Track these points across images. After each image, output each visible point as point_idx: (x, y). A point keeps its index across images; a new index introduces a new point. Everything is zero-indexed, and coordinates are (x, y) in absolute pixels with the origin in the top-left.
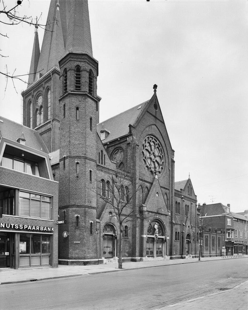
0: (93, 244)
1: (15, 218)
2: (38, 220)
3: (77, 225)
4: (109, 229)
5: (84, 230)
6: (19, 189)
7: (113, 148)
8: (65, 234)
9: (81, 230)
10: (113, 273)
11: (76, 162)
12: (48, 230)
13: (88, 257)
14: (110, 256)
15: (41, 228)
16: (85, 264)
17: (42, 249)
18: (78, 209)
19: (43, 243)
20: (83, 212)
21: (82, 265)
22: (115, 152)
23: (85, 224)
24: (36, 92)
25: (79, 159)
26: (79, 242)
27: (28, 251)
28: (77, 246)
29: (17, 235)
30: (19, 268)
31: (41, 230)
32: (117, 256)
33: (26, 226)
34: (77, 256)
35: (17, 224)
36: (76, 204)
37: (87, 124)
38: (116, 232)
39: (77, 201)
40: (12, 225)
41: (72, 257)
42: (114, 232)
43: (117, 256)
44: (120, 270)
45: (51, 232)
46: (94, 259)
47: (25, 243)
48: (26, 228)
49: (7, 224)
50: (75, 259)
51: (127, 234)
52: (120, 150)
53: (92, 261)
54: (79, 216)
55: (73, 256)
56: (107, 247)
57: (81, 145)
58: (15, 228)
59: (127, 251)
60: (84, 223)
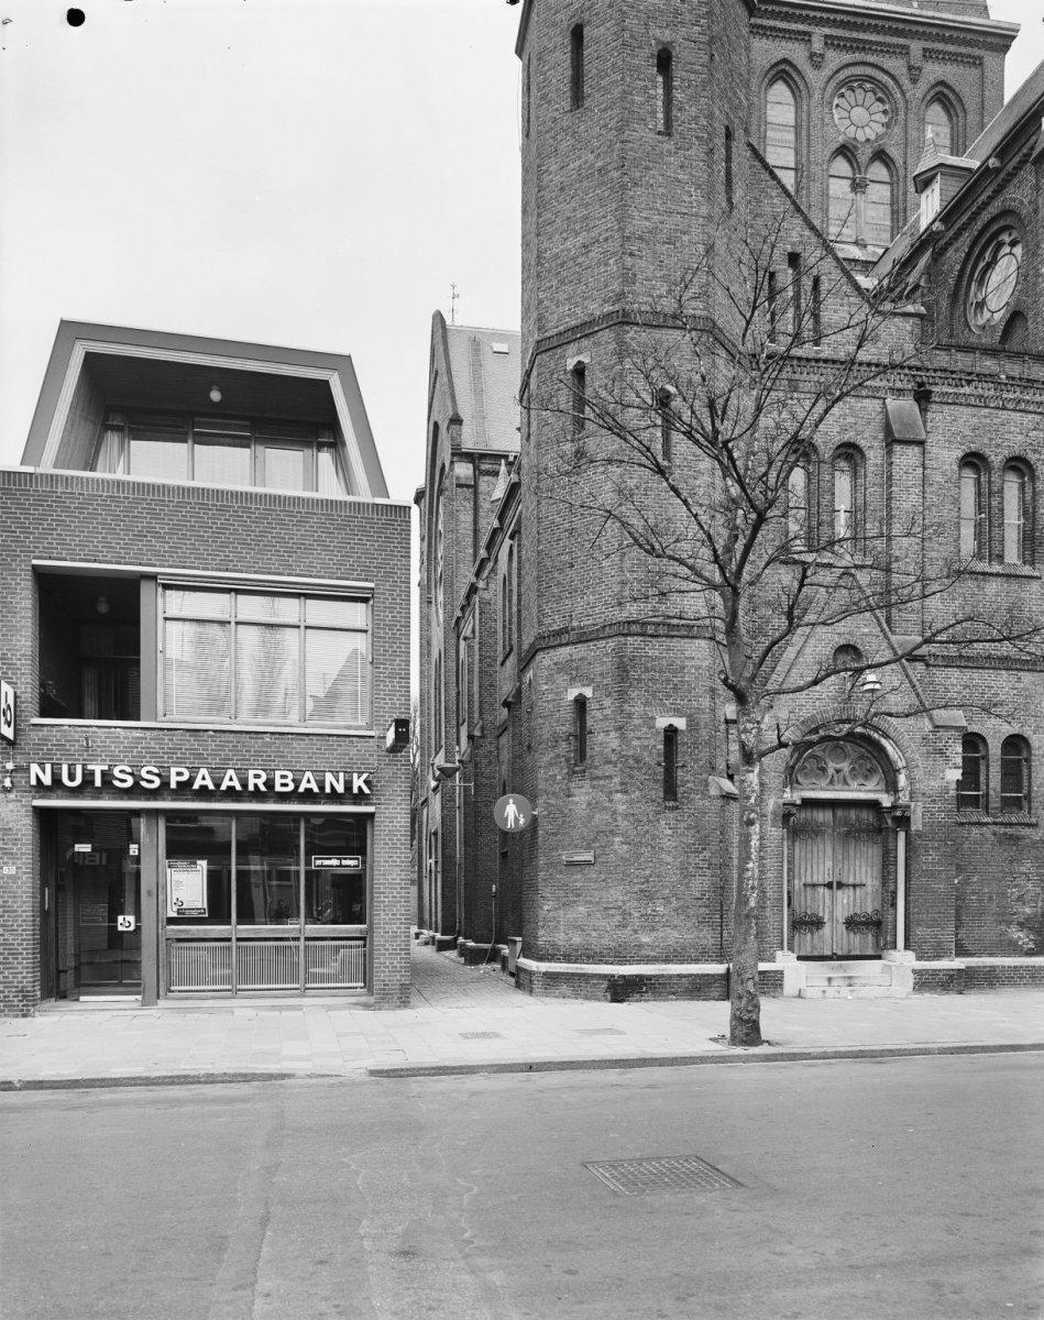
0: (683, 868)
1: (127, 733)
2: (272, 733)
3: (581, 753)
4: (845, 766)
5: (617, 780)
6: (153, 577)
7: (965, 241)
8: (511, 810)
9: (598, 778)
10: (612, 1075)
11: (571, 364)
12: (328, 790)
13: (641, 946)
14: (861, 942)
15: (278, 781)
16: (622, 990)
17: (298, 893)
18: (580, 650)
19: (319, 862)
20: (608, 665)
21: (599, 1000)
22: (982, 265)
23: (623, 737)
24: (848, 57)
25: (585, 342)
26: (589, 857)
27: (217, 910)
28: (577, 880)
29: (148, 826)
30: (161, 1003)
31: (278, 788)
32: (907, 947)
33: (179, 774)
34: (577, 940)
35: (178, 763)
36: (575, 624)
37: (633, 102)
38: (902, 780)
39: (580, 605)
40: (98, 769)
41: (554, 945)
42: (887, 786)
43: (907, 947)
44: (739, 1058)
45: (361, 798)
46: (697, 961)
47: (203, 864)
48: (178, 783)
49: (65, 769)
50: (567, 958)
51: (1030, 792)
52: (1006, 238)
53: (671, 976)
54: (588, 692)
55: (560, 938)
56: (829, 885)
57: (595, 253)
58: (116, 783)
59: (1028, 910)
60: (613, 735)
